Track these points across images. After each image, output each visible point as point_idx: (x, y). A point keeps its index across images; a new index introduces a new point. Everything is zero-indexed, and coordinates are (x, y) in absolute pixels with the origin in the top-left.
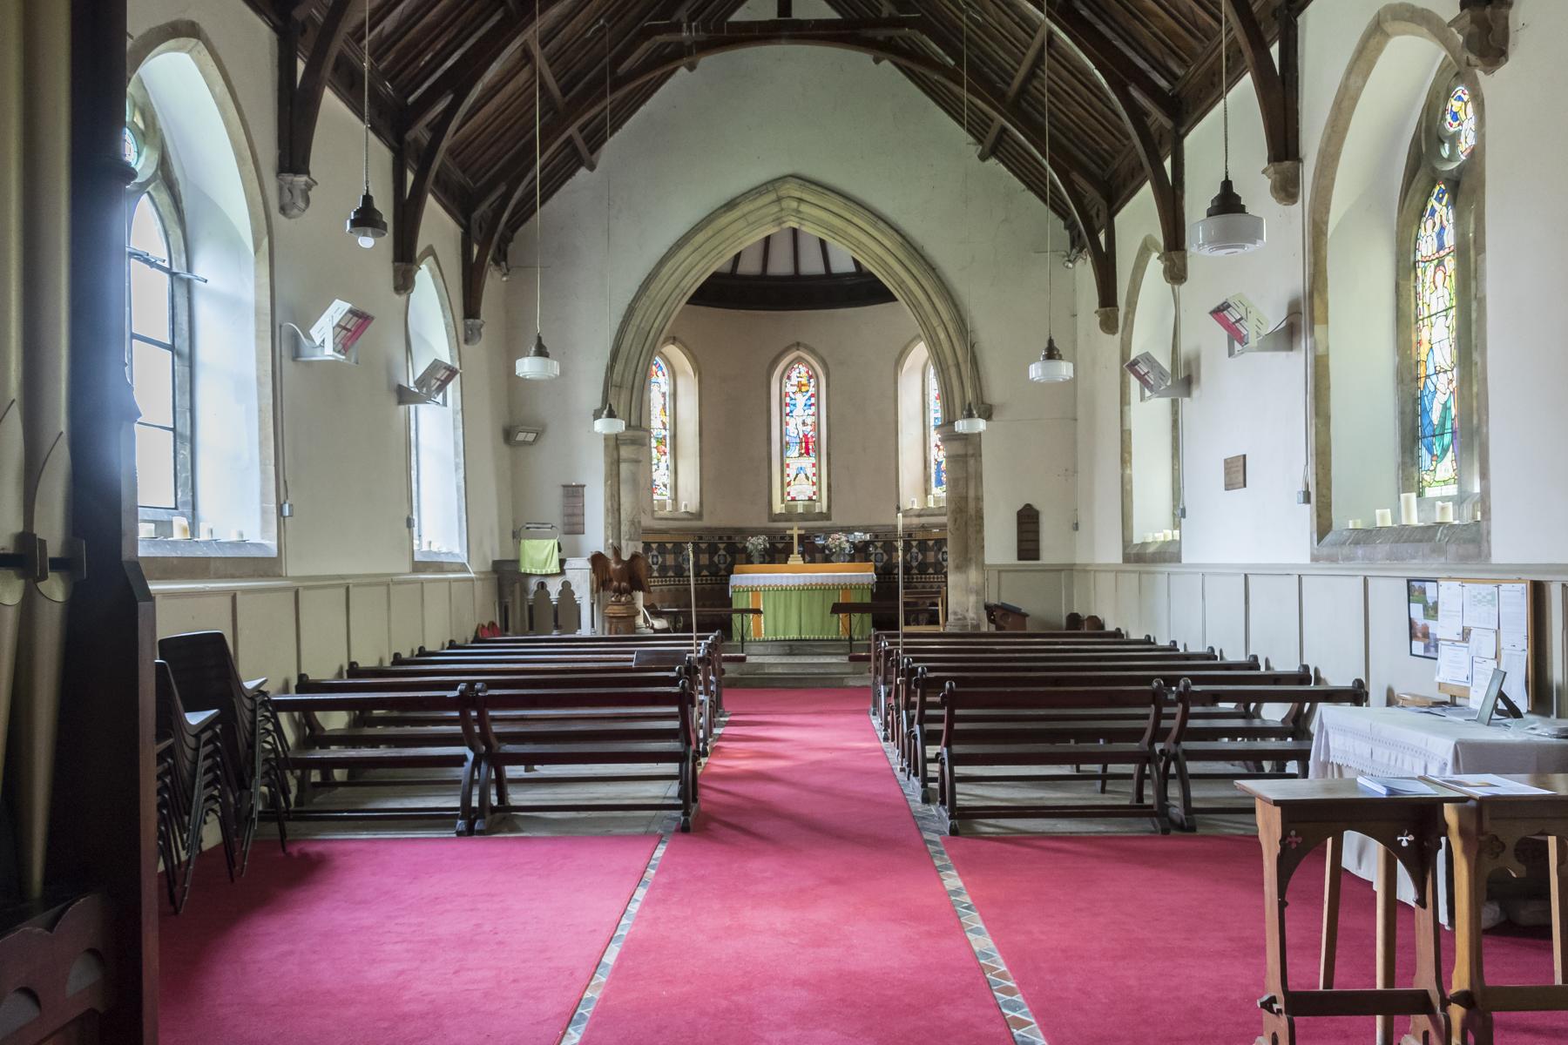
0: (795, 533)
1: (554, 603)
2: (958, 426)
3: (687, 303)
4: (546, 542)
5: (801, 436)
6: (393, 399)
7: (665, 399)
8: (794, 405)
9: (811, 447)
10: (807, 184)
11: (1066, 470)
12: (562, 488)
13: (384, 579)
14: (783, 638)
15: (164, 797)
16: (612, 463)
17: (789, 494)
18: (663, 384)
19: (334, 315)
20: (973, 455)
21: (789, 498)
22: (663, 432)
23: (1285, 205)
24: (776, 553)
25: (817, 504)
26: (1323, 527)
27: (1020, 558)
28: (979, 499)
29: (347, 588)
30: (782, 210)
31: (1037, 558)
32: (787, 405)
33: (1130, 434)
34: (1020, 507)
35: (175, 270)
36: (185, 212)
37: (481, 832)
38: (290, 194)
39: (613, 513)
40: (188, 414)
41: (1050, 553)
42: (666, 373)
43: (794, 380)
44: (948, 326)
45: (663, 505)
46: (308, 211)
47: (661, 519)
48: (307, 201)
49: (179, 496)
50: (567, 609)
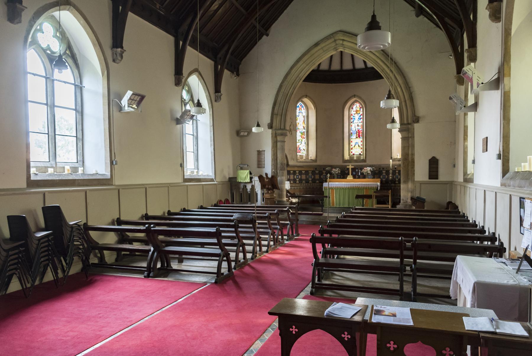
0: (350, 167)
1: (249, 193)
2: (388, 127)
3: (304, 81)
4: (245, 171)
5: (357, 130)
6: (174, 123)
7: (304, 118)
8: (354, 119)
9: (360, 134)
10: (345, 34)
11: (451, 143)
12: (257, 152)
13: (167, 185)
14: (342, 207)
15: (19, 261)
16: (274, 143)
17: (352, 152)
18: (304, 113)
19: (128, 96)
20: (411, 137)
21: (352, 154)
22: (304, 130)
23: (495, 23)
24: (343, 175)
25: (362, 156)
26: (505, 170)
27: (430, 179)
28: (413, 154)
29: (145, 188)
30: (337, 45)
31: (437, 179)
32: (352, 119)
33: (467, 127)
34: (430, 158)
35: (76, 84)
36: (79, 64)
37: (152, 277)
38: (116, 56)
39: (274, 161)
40: (81, 131)
41: (443, 176)
42: (305, 108)
43: (354, 109)
44: (401, 85)
45: (301, 157)
46: (123, 60)
47: (300, 162)
48: (122, 57)
49: (78, 159)
50: (251, 196)
